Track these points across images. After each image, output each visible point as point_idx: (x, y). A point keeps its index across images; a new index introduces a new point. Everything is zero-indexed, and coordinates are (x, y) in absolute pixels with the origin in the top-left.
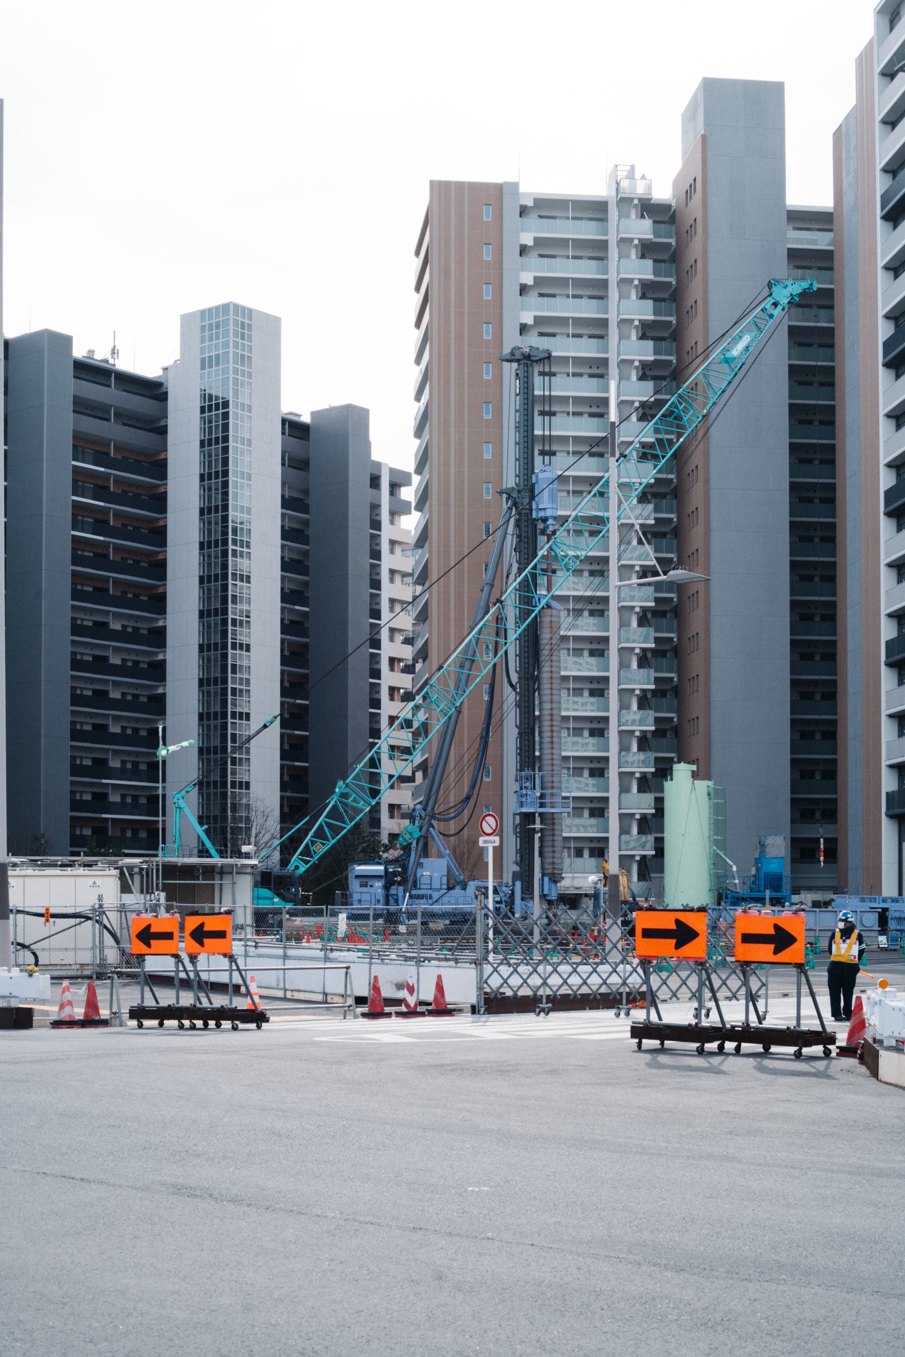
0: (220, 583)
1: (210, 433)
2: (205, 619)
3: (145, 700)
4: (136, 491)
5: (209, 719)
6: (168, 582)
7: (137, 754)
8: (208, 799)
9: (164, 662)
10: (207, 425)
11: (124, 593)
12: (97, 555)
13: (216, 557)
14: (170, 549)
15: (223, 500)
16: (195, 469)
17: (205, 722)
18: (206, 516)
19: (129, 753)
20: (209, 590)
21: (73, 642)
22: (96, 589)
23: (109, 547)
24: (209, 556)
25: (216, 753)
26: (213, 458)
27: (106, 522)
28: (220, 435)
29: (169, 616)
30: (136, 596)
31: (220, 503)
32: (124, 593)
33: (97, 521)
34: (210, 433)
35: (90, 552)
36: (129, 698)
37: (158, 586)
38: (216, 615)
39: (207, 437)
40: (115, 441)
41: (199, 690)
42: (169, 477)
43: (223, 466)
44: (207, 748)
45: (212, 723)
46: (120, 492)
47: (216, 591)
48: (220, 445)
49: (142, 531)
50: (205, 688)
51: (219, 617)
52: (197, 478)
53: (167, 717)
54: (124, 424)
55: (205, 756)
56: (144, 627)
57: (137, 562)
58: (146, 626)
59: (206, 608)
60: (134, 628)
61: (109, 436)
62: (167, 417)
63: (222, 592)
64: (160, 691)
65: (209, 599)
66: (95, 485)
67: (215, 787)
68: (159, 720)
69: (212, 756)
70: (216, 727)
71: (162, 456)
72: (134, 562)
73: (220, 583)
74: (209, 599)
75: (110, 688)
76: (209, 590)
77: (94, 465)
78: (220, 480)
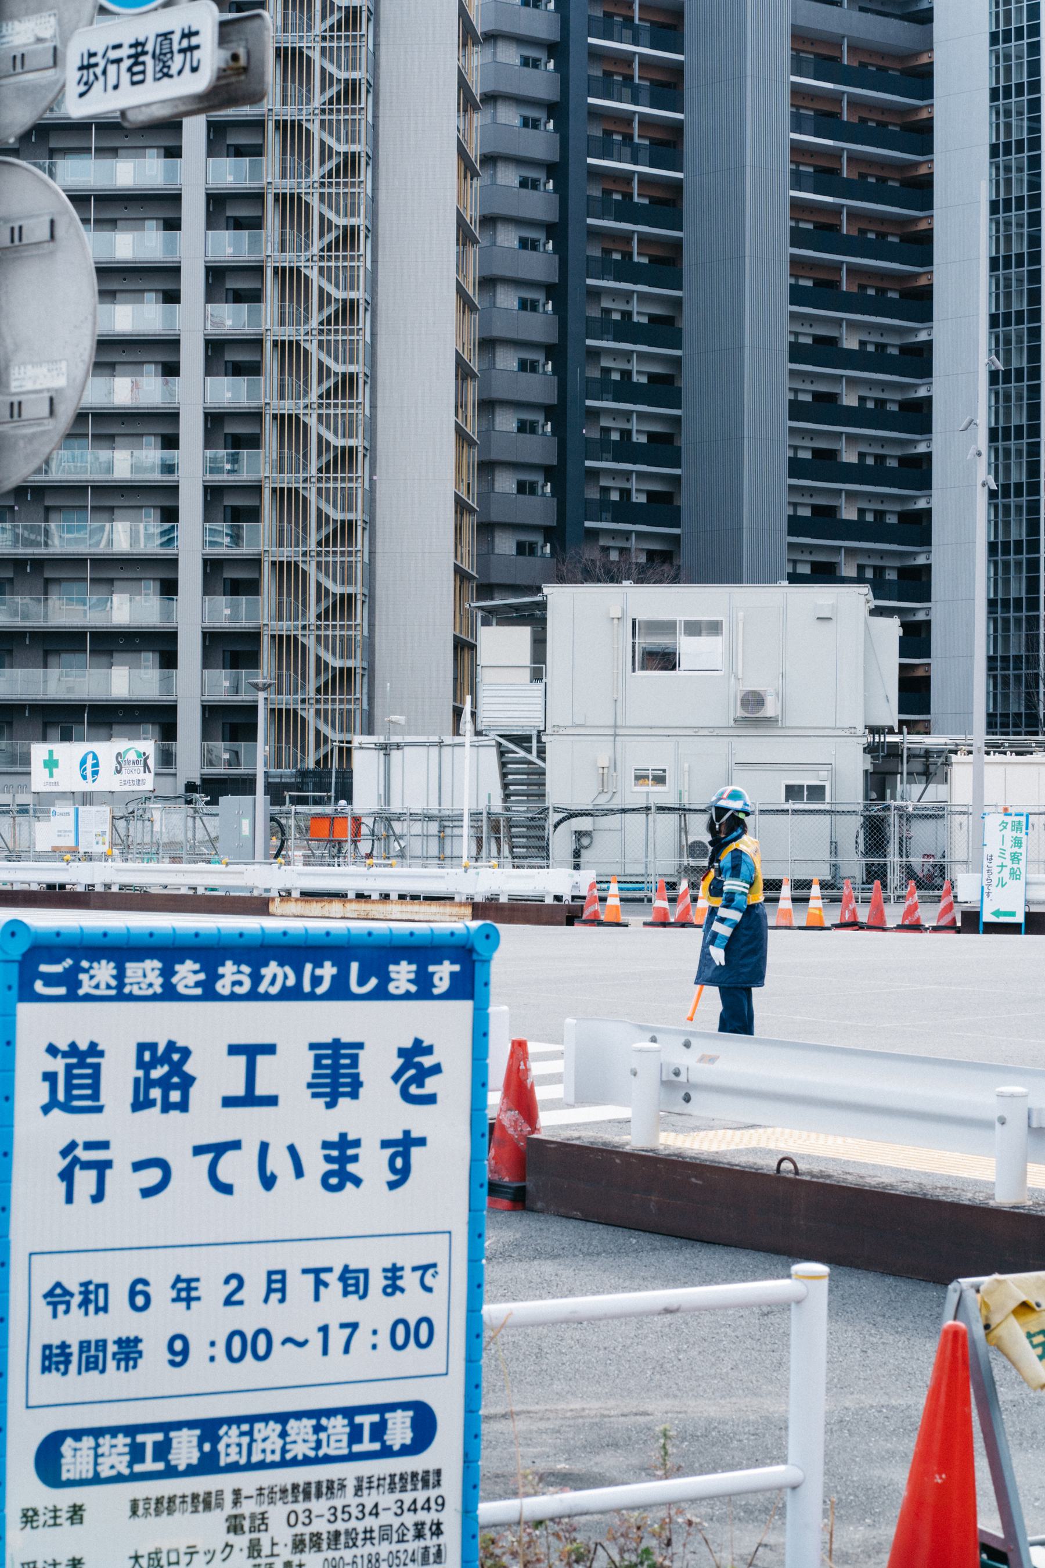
0: (1026, 211)
1: (1008, 20)
2: (1001, 329)
3: (895, 351)
4: (880, 118)
5: (1006, 551)
6: (935, 268)
7: (882, 554)
8: (1006, 628)
9: (928, 456)
10: (1001, 8)
11: (863, 287)
12: (818, 226)
13: (1020, 170)
14: (938, 211)
15: (1031, 130)
16: (982, 475)
17: (1000, 558)
18: (1001, 158)
19: (871, 440)
20: (1008, 279)
21: (791, 545)
22: (818, 226)
23: (841, 269)
24: (1007, 224)
25: (1018, 551)
26: (1013, 62)
27: (836, 60)
28: (1025, 24)
29: (936, 323)
30: (881, 291)
31: (1025, 136)
32: (863, 287)
33: (820, 170)
34: (1008, 20)
35: (809, 278)
36: (870, 405)
37: (919, 109)
38: (1020, 264)
39: (1002, 83)
40: (848, 37)
41: (988, 676)
42: (934, 318)
43: (1029, 76)
44: (1004, 372)
45: (1012, 444)
46: (856, 64)
47: (1020, 281)
48: (1026, 41)
49: (890, 183)
50: (1000, 444)
51: (1025, 326)
52: (986, 39)
53: (934, 492)
54: (862, 9)
55: (1000, 558)
56: (893, 344)
57: (882, 236)
58: (898, 397)
59: (1001, 424)
60: (877, 345)
61: (841, 31)
62: (932, 50)
63: (1030, 282)
64: (922, 448)
65: (1008, 295)
66: (816, 111)
67: (1018, 607)
68: (918, 497)
69: (1012, 557)
70: (1019, 508)
71: (924, 59)
72: (877, 180)
73: (1026, 211)
74: (1008, 295)
75: (842, 558)
76: (1008, 279)
77: (816, 79)
78: (1026, 97)
